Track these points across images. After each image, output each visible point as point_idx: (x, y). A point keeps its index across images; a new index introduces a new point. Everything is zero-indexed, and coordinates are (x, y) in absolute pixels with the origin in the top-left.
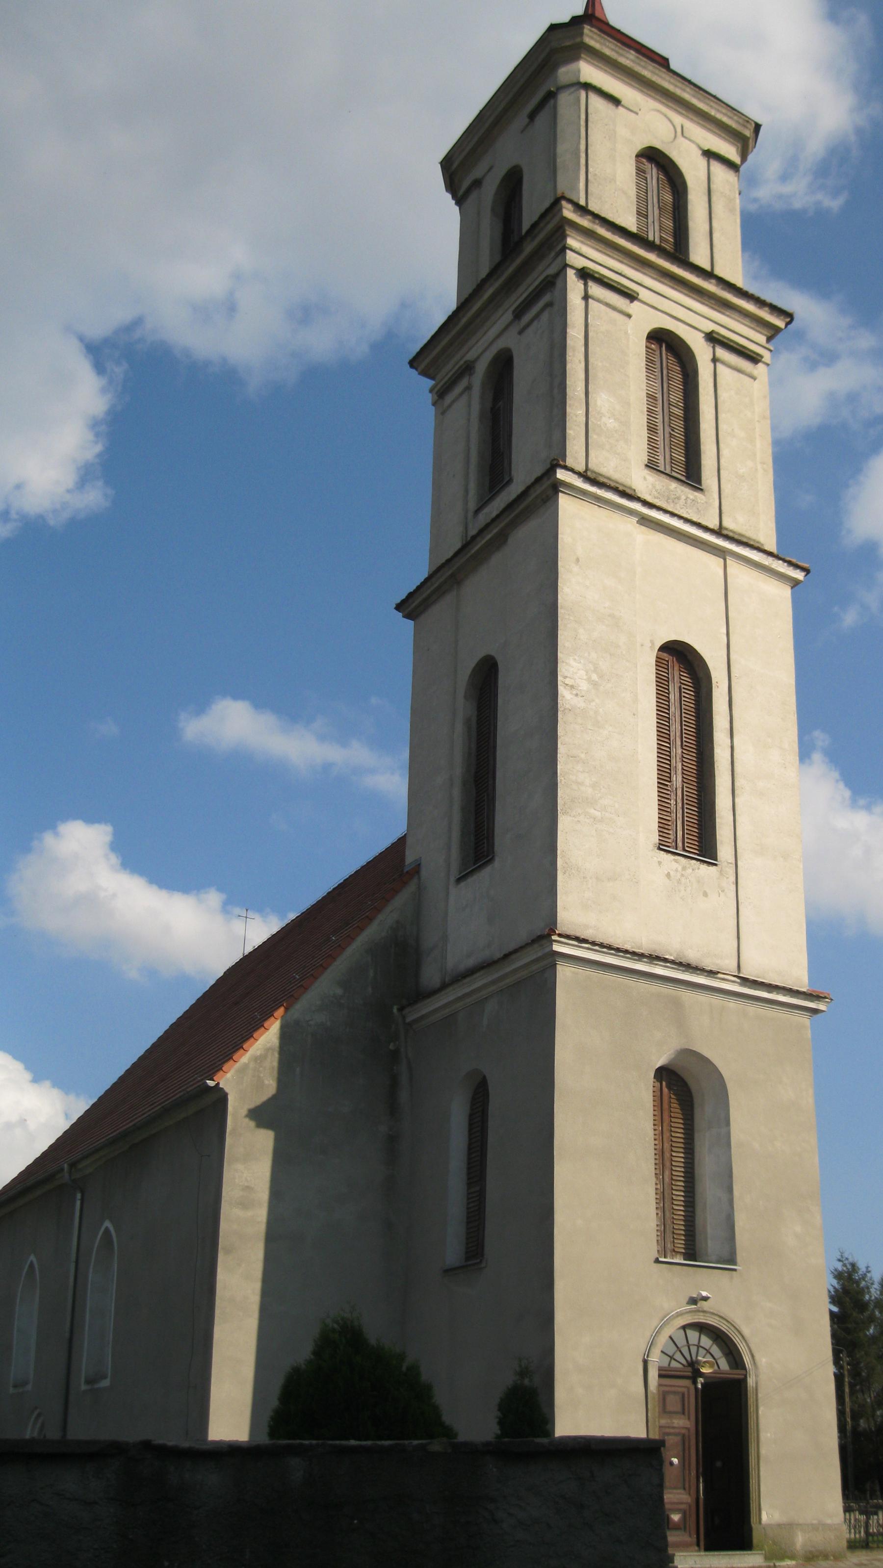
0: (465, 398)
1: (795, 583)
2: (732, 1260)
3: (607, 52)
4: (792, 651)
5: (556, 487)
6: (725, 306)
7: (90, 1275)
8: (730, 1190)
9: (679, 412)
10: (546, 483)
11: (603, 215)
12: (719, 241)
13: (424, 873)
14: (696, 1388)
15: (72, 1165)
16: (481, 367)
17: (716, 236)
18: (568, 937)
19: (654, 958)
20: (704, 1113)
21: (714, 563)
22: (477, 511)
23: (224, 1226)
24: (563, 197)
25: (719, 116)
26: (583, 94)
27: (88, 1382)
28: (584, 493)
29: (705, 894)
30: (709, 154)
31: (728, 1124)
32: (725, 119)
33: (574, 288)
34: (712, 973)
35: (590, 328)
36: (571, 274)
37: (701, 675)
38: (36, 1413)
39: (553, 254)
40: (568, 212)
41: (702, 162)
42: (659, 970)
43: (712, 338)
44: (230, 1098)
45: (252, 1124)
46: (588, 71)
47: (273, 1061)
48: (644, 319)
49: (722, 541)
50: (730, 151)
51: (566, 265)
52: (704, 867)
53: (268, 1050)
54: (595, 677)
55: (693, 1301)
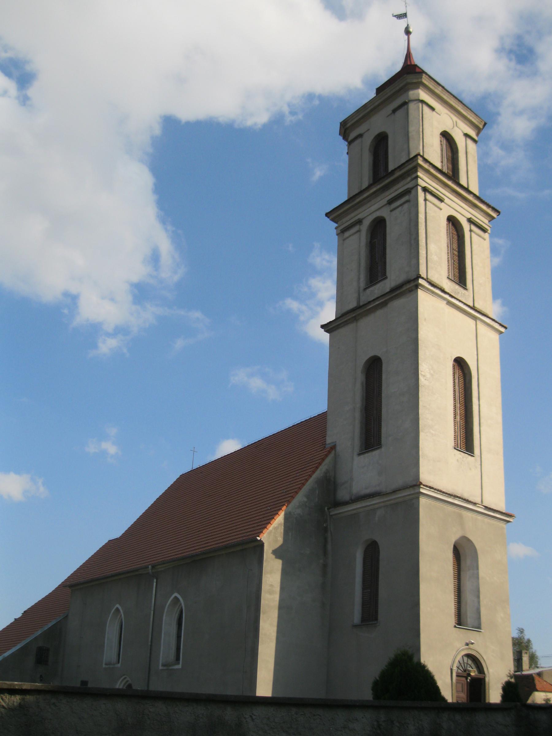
0: (356, 236)
1: (501, 333)
2: (479, 627)
3: (431, 87)
4: (499, 363)
5: (417, 286)
6: (475, 206)
7: (164, 618)
8: (478, 597)
9: (456, 253)
10: (412, 284)
11: (434, 164)
12: (470, 175)
13: (338, 448)
14: (467, 681)
15: (153, 567)
16: (367, 223)
17: (469, 173)
18: (427, 486)
19: (455, 497)
20: (466, 563)
21: (472, 322)
22: (365, 289)
23: (263, 602)
24: (419, 154)
25: (471, 118)
26: (420, 105)
27: (164, 665)
28: (428, 289)
29: (470, 469)
30: (466, 135)
31: (478, 569)
32: (473, 120)
33: (421, 195)
34: (475, 504)
35: (428, 215)
36: (419, 189)
37: (466, 372)
38: (123, 677)
39: (409, 179)
40: (420, 161)
41: (463, 138)
42: (456, 502)
43: (470, 221)
44: (265, 545)
45: (274, 557)
46: (423, 95)
47: (281, 529)
48: (447, 211)
49: (474, 312)
50: (473, 134)
51: (417, 185)
52: (470, 457)
53: (280, 524)
54: (432, 372)
55: (467, 644)
